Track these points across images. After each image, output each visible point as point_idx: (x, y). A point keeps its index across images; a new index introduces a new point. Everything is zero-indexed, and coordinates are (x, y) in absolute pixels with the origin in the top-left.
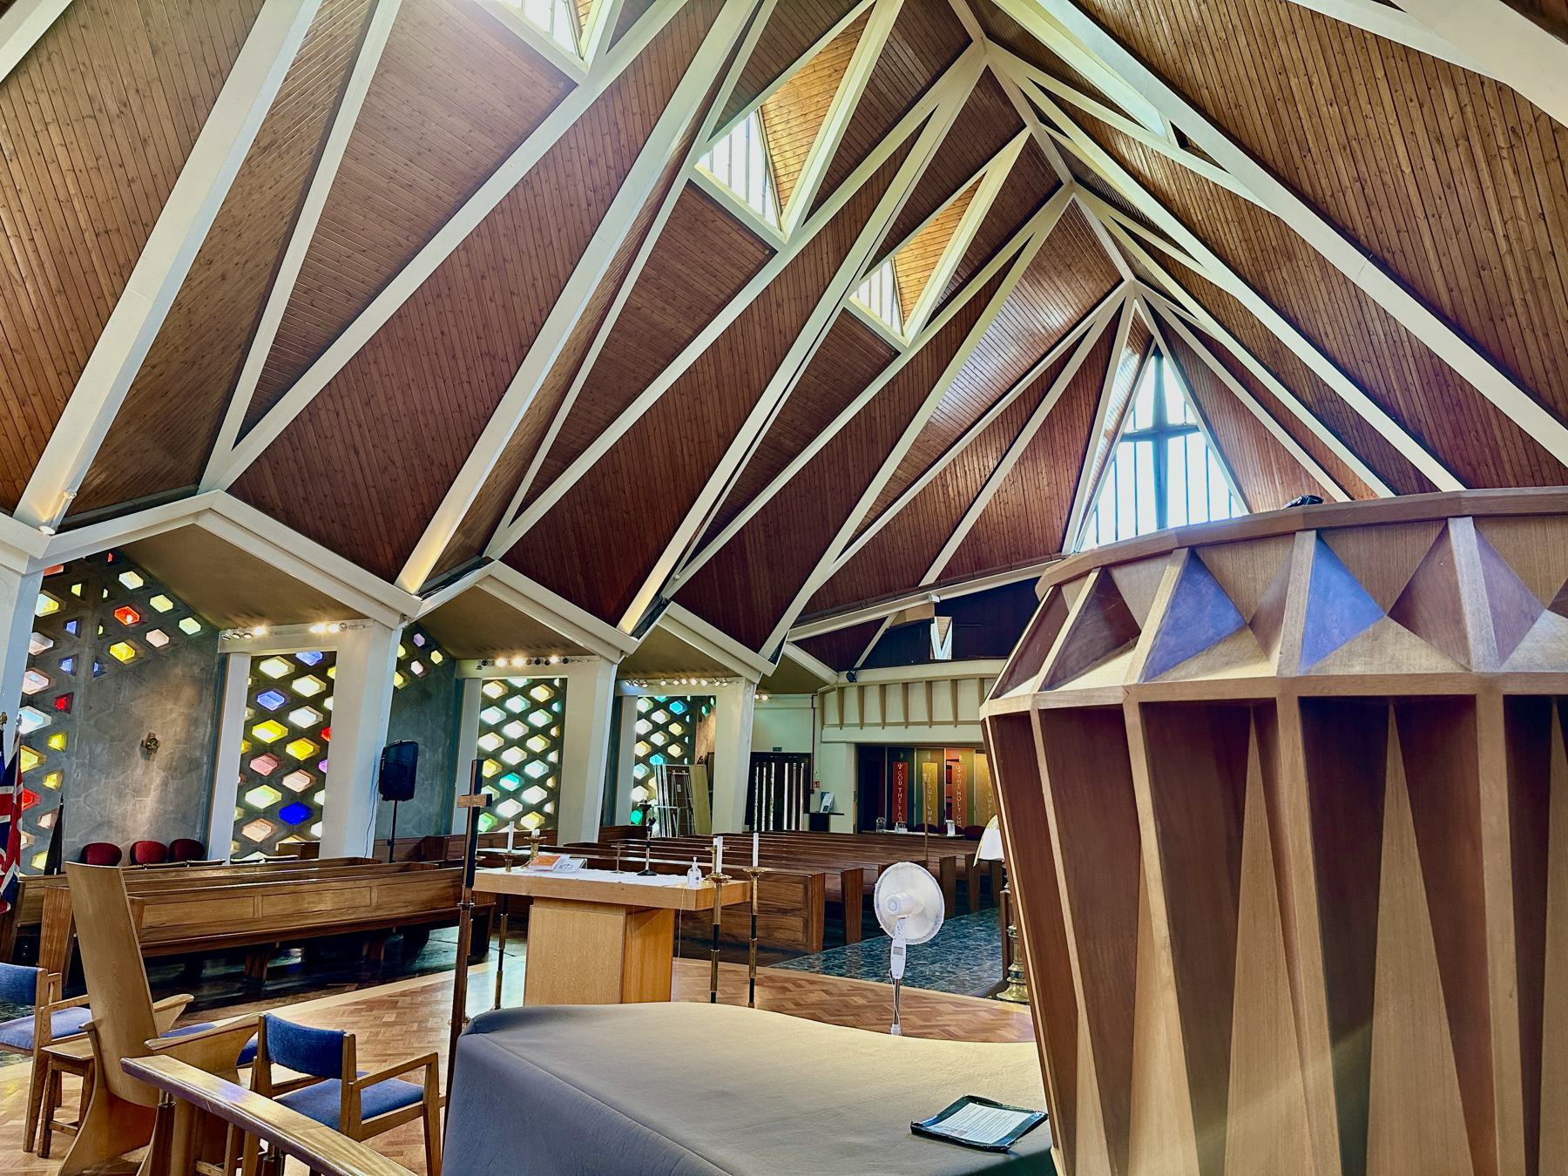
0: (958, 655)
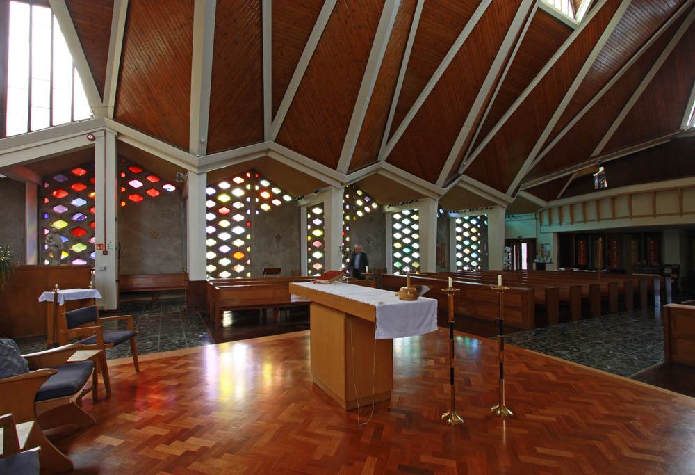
0: (610, 187)
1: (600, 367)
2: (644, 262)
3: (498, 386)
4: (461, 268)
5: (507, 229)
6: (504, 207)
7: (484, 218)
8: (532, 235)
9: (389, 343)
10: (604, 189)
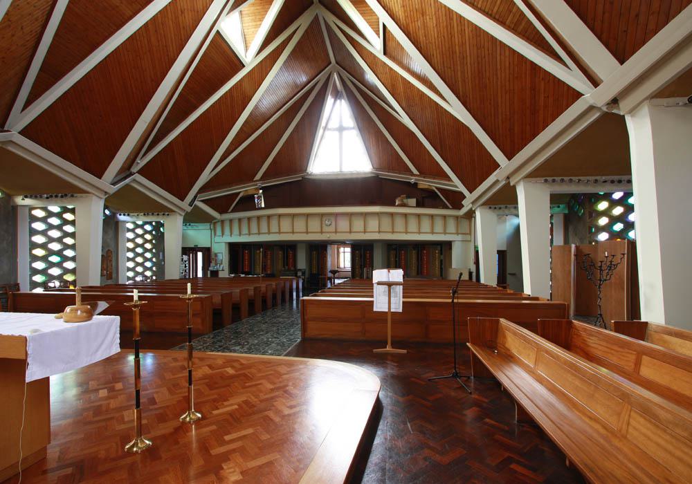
0: (267, 207)
1: (263, 353)
2: (287, 267)
3: (187, 394)
4: (133, 278)
5: (184, 237)
6: (181, 215)
7: (160, 225)
8: (206, 244)
9: (46, 381)
10: (262, 208)
